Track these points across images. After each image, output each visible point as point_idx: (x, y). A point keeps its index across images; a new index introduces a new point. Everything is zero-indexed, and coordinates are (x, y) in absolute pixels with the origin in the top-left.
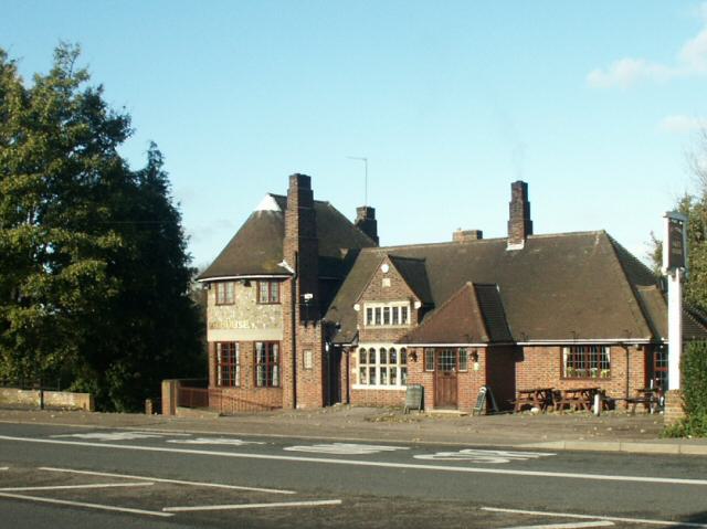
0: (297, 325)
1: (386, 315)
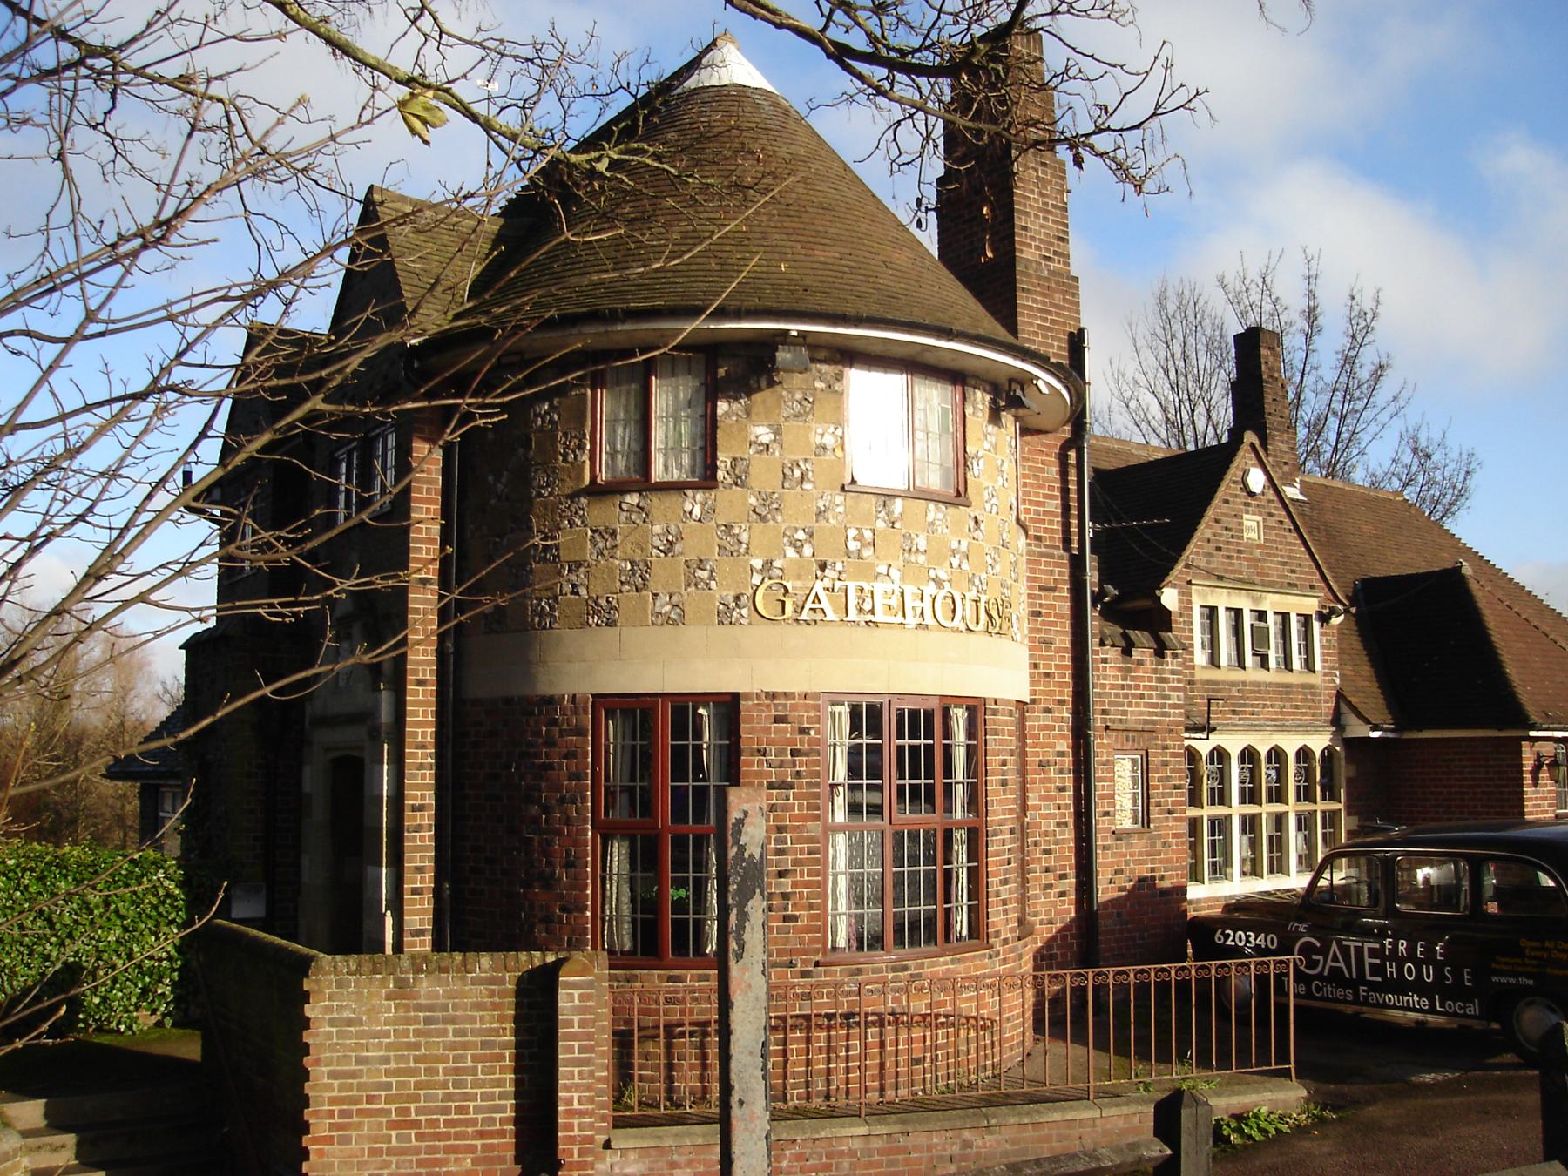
0: (1093, 643)
1: (1261, 637)
